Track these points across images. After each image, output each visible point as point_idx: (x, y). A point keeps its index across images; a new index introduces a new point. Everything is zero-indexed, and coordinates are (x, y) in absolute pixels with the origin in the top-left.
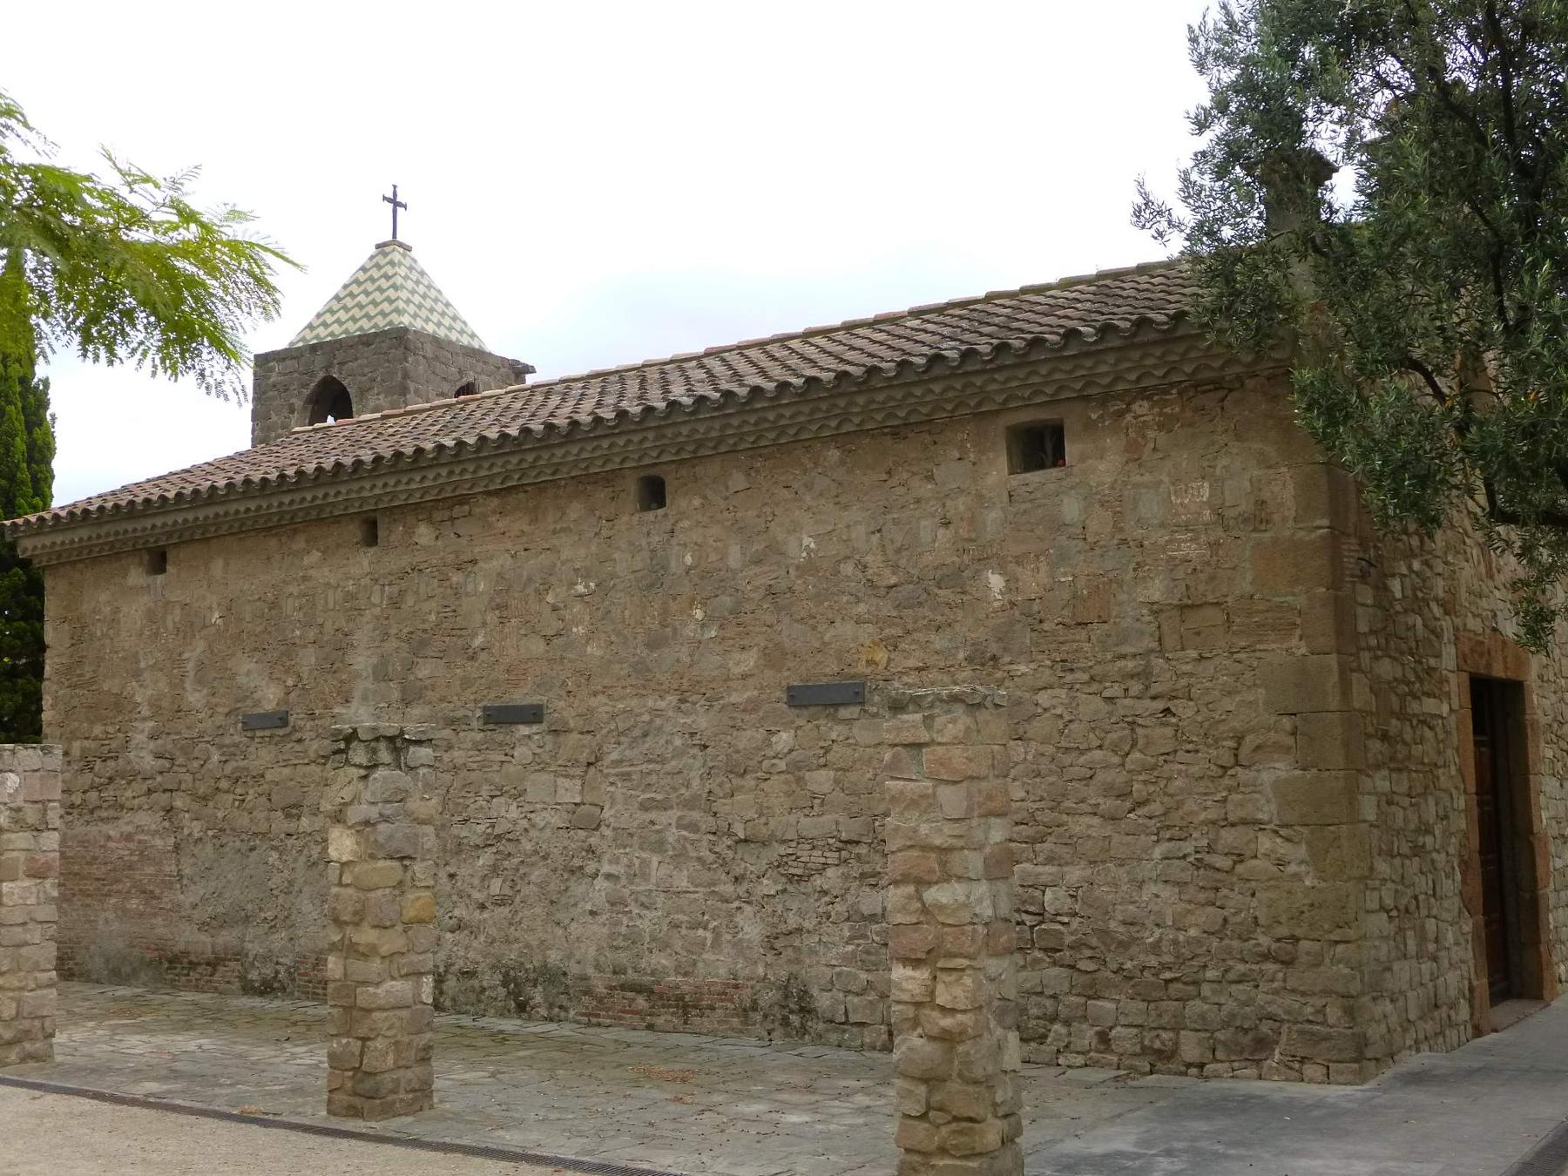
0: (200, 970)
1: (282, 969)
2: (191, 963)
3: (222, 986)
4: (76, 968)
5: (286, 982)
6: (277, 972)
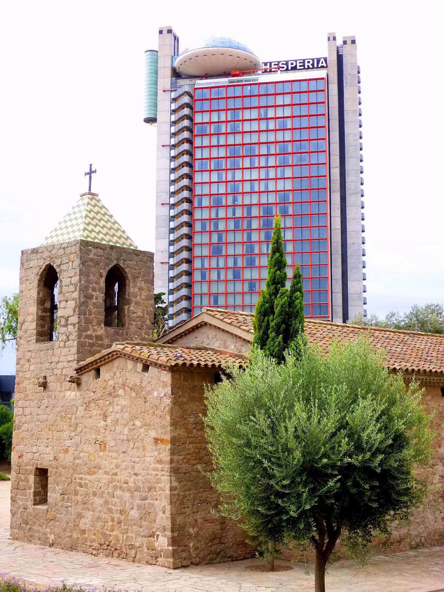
0: (394, 545)
1: (423, 538)
2: (391, 543)
3: (403, 549)
4: (342, 556)
5: (425, 542)
6: (421, 540)
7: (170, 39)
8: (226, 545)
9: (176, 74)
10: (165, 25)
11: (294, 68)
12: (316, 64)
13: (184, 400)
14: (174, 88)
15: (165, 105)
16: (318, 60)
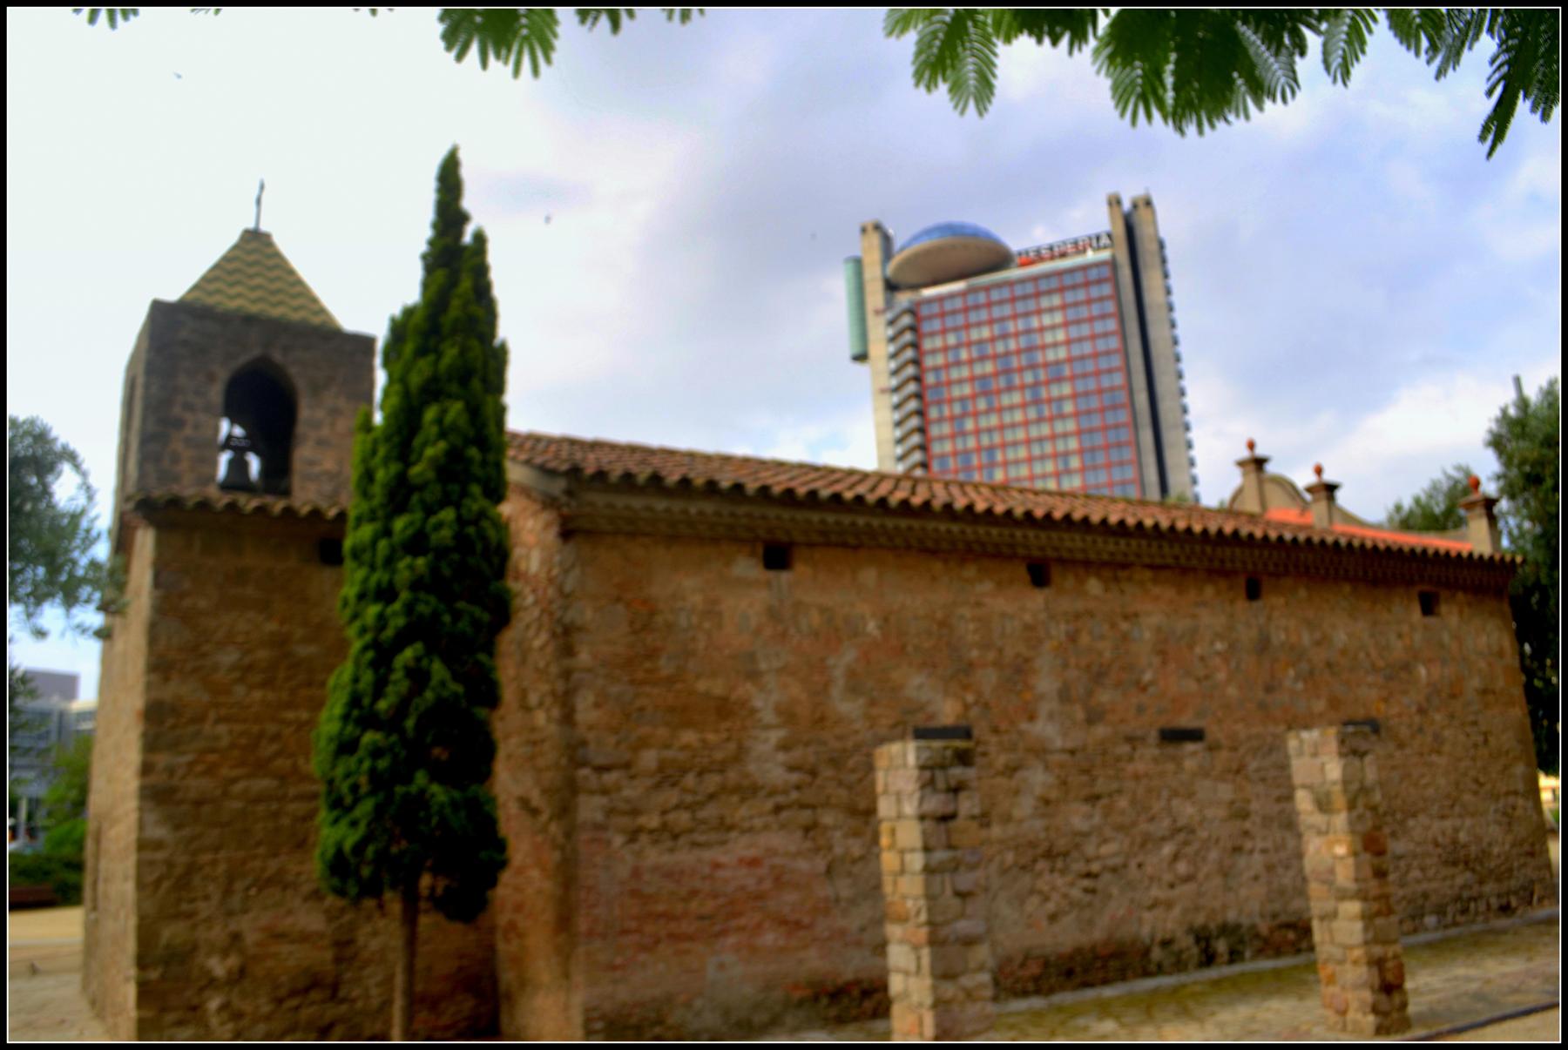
7: (875, 239)
8: (359, 1004)
9: (891, 287)
10: (869, 218)
11: (1063, 255)
12: (1095, 241)
13: (203, 604)
14: (889, 304)
15: (879, 331)
16: (1098, 238)
